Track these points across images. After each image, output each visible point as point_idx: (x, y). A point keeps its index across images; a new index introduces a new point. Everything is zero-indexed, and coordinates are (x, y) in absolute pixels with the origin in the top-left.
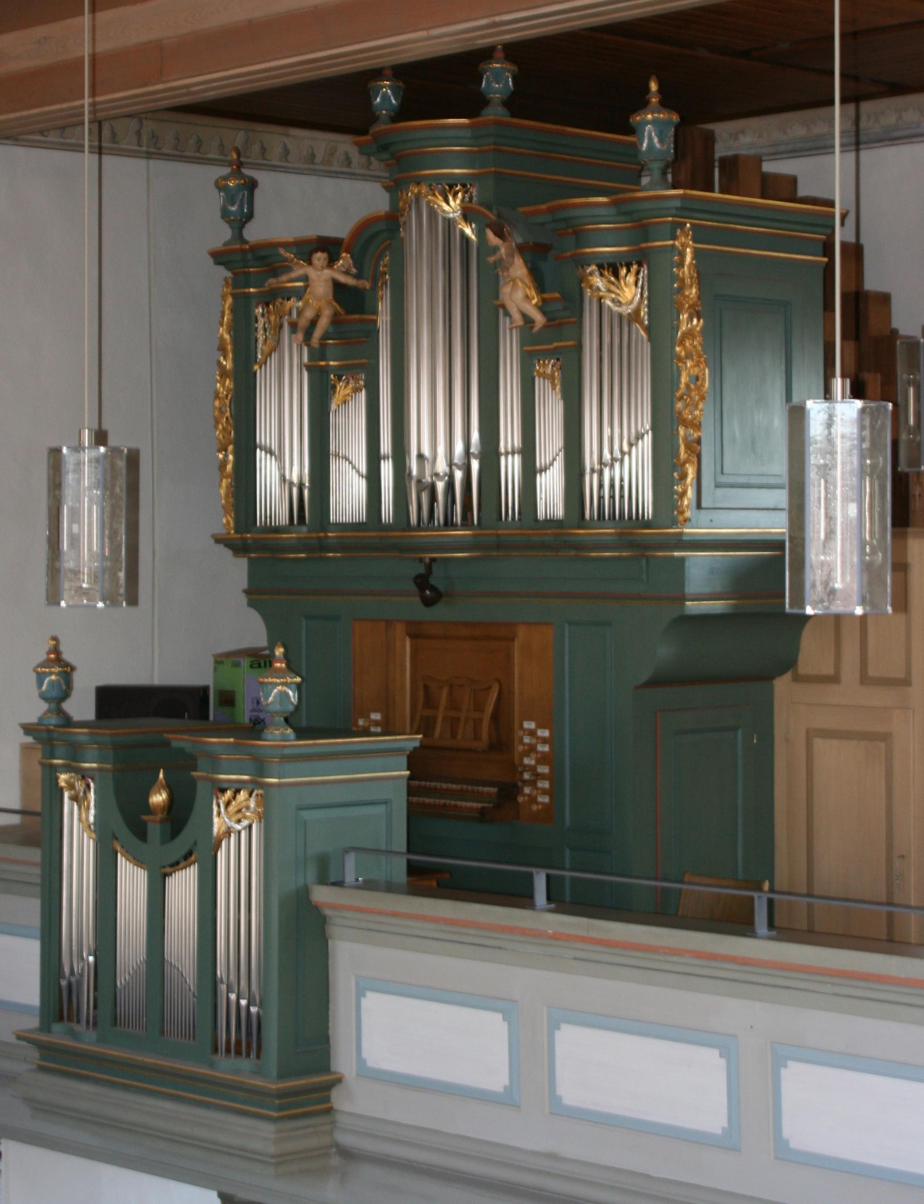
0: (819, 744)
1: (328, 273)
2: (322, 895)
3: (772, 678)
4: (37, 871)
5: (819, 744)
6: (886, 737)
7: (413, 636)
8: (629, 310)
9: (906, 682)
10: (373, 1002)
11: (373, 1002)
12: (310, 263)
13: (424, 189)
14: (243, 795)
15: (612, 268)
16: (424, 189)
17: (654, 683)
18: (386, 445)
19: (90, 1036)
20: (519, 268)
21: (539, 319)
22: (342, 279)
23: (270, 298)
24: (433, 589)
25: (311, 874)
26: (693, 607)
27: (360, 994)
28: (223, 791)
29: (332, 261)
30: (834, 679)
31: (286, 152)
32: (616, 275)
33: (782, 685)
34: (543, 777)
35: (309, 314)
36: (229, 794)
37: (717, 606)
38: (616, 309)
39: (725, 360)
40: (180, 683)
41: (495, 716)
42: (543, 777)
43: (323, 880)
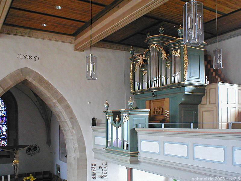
0: (204, 112)
1: (142, 58)
2: (136, 129)
3: (198, 105)
4: (105, 130)
5: (204, 112)
6: (212, 111)
7: (153, 102)
8: (178, 55)
9: (216, 103)
10: (143, 142)
11: (143, 142)
12: (139, 57)
13: (153, 45)
14: (127, 116)
15: (176, 50)
16: (153, 45)
17: (181, 104)
18: (149, 79)
19: (110, 148)
20: (163, 52)
21: (166, 58)
22: (144, 58)
23: (136, 63)
24: (154, 95)
25: (135, 126)
26: (186, 93)
27: (141, 142)
28: (124, 116)
29: (142, 56)
30: (206, 104)
31: (141, 51)
32: (176, 51)
33: (199, 105)
34: (168, 117)
35: (140, 63)
36: (125, 117)
37: (190, 93)
38: (176, 56)
39: (191, 64)
40: (59, 43)
41: (162, 111)
42: (168, 119)
43: (137, 127)
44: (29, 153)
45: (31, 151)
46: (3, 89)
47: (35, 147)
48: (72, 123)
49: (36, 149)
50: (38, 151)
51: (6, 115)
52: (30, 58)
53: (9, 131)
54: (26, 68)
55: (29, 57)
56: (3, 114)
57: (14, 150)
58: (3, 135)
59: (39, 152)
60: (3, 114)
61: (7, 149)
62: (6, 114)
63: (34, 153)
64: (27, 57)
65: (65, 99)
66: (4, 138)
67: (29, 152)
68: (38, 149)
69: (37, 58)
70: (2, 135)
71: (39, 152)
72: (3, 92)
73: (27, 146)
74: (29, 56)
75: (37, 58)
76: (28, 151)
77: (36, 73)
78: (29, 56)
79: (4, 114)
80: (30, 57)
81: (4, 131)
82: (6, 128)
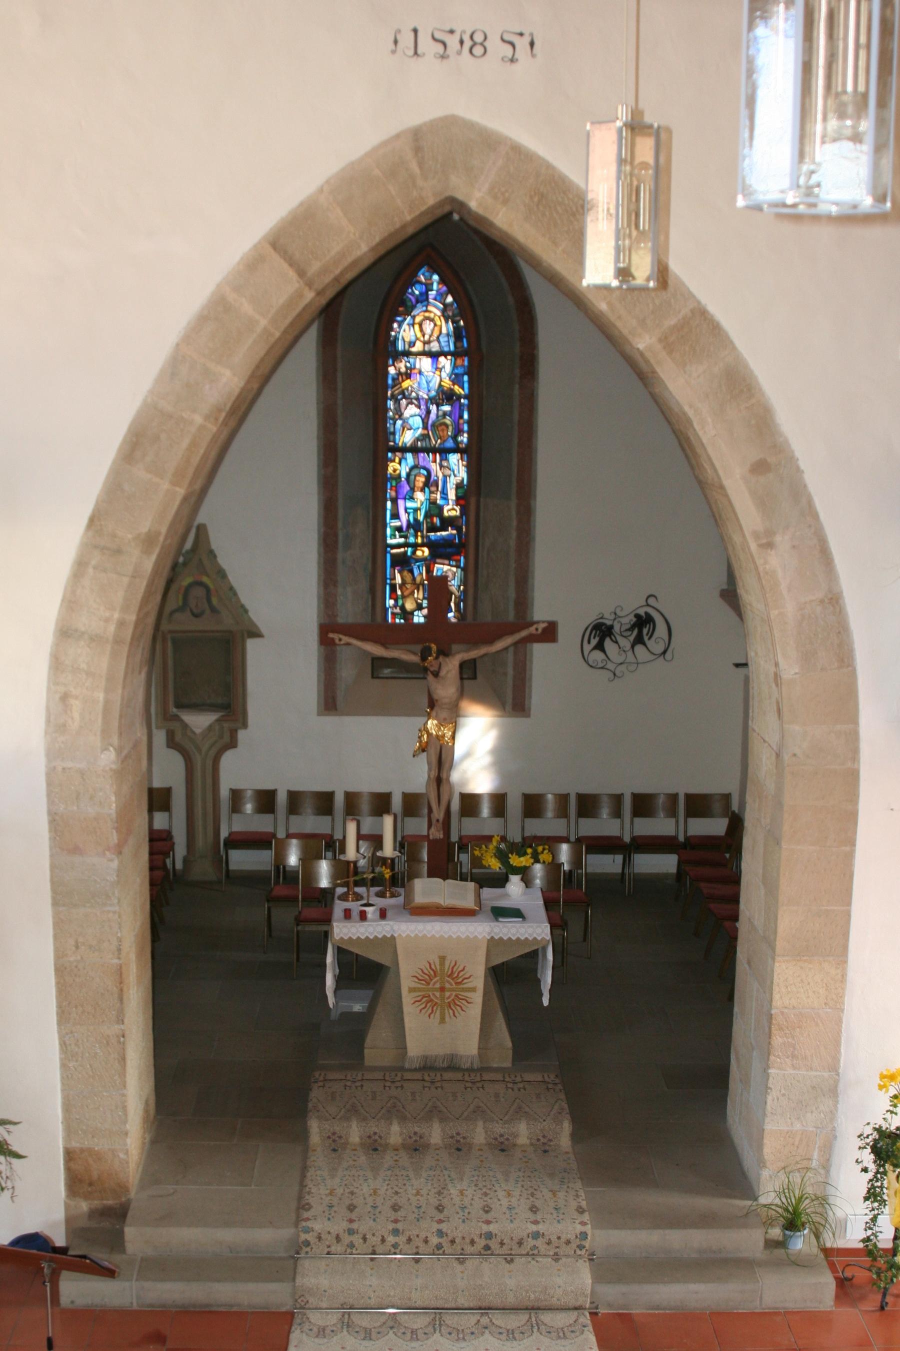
44: (598, 655)
45: (608, 643)
46: (301, 273)
47: (637, 616)
48: (765, 502)
49: (645, 631)
50: (659, 648)
51: (466, 386)
52: (478, 50)
53: (479, 495)
54: (450, 122)
55: (468, 43)
56: (447, 383)
57: (424, 656)
58: (447, 523)
59: (664, 652)
60: (447, 383)
61: (384, 644)
62: (466, 378)
63: (630, 657)
64: (453, 42)
65: (715, 328)
66: (447, 543)
67: (600, 647)
68: (661, 630)
69: (522, 44)
70: (437, 521)
71: (664, 652)
72: (299, 295)
73: (512, 633)
74: (466, 38)
75: (522, 44)
76: (594, 642)
77: (517, 150)
78: (466, 38)
79: (456, 379)
80: (479, 38)
81: (452, 495)
82: (462, 474)
